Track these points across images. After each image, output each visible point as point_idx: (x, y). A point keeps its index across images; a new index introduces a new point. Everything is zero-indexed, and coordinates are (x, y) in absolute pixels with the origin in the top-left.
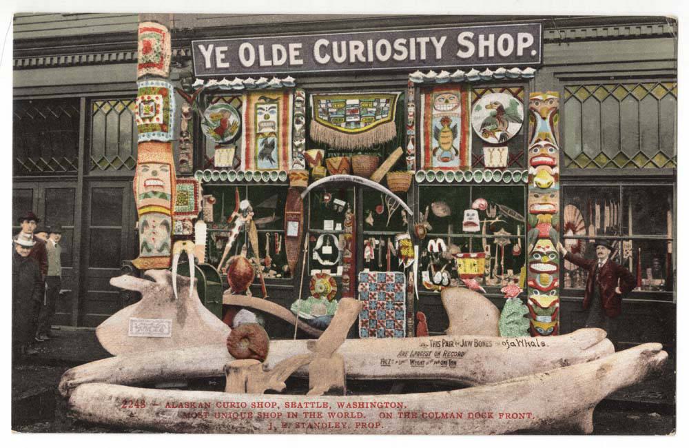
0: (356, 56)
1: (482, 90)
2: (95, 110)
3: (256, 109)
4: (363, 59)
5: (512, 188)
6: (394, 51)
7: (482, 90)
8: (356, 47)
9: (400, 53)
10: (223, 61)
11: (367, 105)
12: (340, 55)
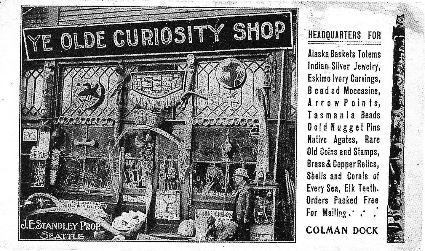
0: (147, 41)
2: (65, 75)
6: (175, 36)
8: (147, 34)
9: (180, 38)
10: (48, 45)
11: (166, 79)
12: (133, 41)
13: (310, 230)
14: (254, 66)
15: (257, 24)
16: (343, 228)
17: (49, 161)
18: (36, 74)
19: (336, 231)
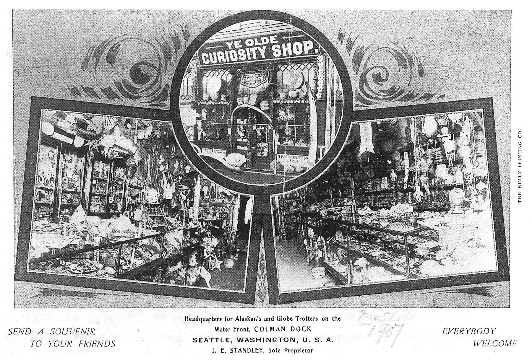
1: (300, 64)
3: (104, 116)
4: (225, 61)
5: (254, 212)
7: (300, 64)
13: (257, 329)
14: (309, 66)
15: (277, 42)
16: (243, 349)
17: (196, 126)
18: (222, 73)
19: (239, 351)
